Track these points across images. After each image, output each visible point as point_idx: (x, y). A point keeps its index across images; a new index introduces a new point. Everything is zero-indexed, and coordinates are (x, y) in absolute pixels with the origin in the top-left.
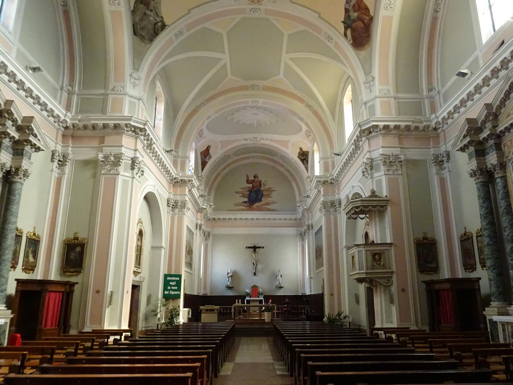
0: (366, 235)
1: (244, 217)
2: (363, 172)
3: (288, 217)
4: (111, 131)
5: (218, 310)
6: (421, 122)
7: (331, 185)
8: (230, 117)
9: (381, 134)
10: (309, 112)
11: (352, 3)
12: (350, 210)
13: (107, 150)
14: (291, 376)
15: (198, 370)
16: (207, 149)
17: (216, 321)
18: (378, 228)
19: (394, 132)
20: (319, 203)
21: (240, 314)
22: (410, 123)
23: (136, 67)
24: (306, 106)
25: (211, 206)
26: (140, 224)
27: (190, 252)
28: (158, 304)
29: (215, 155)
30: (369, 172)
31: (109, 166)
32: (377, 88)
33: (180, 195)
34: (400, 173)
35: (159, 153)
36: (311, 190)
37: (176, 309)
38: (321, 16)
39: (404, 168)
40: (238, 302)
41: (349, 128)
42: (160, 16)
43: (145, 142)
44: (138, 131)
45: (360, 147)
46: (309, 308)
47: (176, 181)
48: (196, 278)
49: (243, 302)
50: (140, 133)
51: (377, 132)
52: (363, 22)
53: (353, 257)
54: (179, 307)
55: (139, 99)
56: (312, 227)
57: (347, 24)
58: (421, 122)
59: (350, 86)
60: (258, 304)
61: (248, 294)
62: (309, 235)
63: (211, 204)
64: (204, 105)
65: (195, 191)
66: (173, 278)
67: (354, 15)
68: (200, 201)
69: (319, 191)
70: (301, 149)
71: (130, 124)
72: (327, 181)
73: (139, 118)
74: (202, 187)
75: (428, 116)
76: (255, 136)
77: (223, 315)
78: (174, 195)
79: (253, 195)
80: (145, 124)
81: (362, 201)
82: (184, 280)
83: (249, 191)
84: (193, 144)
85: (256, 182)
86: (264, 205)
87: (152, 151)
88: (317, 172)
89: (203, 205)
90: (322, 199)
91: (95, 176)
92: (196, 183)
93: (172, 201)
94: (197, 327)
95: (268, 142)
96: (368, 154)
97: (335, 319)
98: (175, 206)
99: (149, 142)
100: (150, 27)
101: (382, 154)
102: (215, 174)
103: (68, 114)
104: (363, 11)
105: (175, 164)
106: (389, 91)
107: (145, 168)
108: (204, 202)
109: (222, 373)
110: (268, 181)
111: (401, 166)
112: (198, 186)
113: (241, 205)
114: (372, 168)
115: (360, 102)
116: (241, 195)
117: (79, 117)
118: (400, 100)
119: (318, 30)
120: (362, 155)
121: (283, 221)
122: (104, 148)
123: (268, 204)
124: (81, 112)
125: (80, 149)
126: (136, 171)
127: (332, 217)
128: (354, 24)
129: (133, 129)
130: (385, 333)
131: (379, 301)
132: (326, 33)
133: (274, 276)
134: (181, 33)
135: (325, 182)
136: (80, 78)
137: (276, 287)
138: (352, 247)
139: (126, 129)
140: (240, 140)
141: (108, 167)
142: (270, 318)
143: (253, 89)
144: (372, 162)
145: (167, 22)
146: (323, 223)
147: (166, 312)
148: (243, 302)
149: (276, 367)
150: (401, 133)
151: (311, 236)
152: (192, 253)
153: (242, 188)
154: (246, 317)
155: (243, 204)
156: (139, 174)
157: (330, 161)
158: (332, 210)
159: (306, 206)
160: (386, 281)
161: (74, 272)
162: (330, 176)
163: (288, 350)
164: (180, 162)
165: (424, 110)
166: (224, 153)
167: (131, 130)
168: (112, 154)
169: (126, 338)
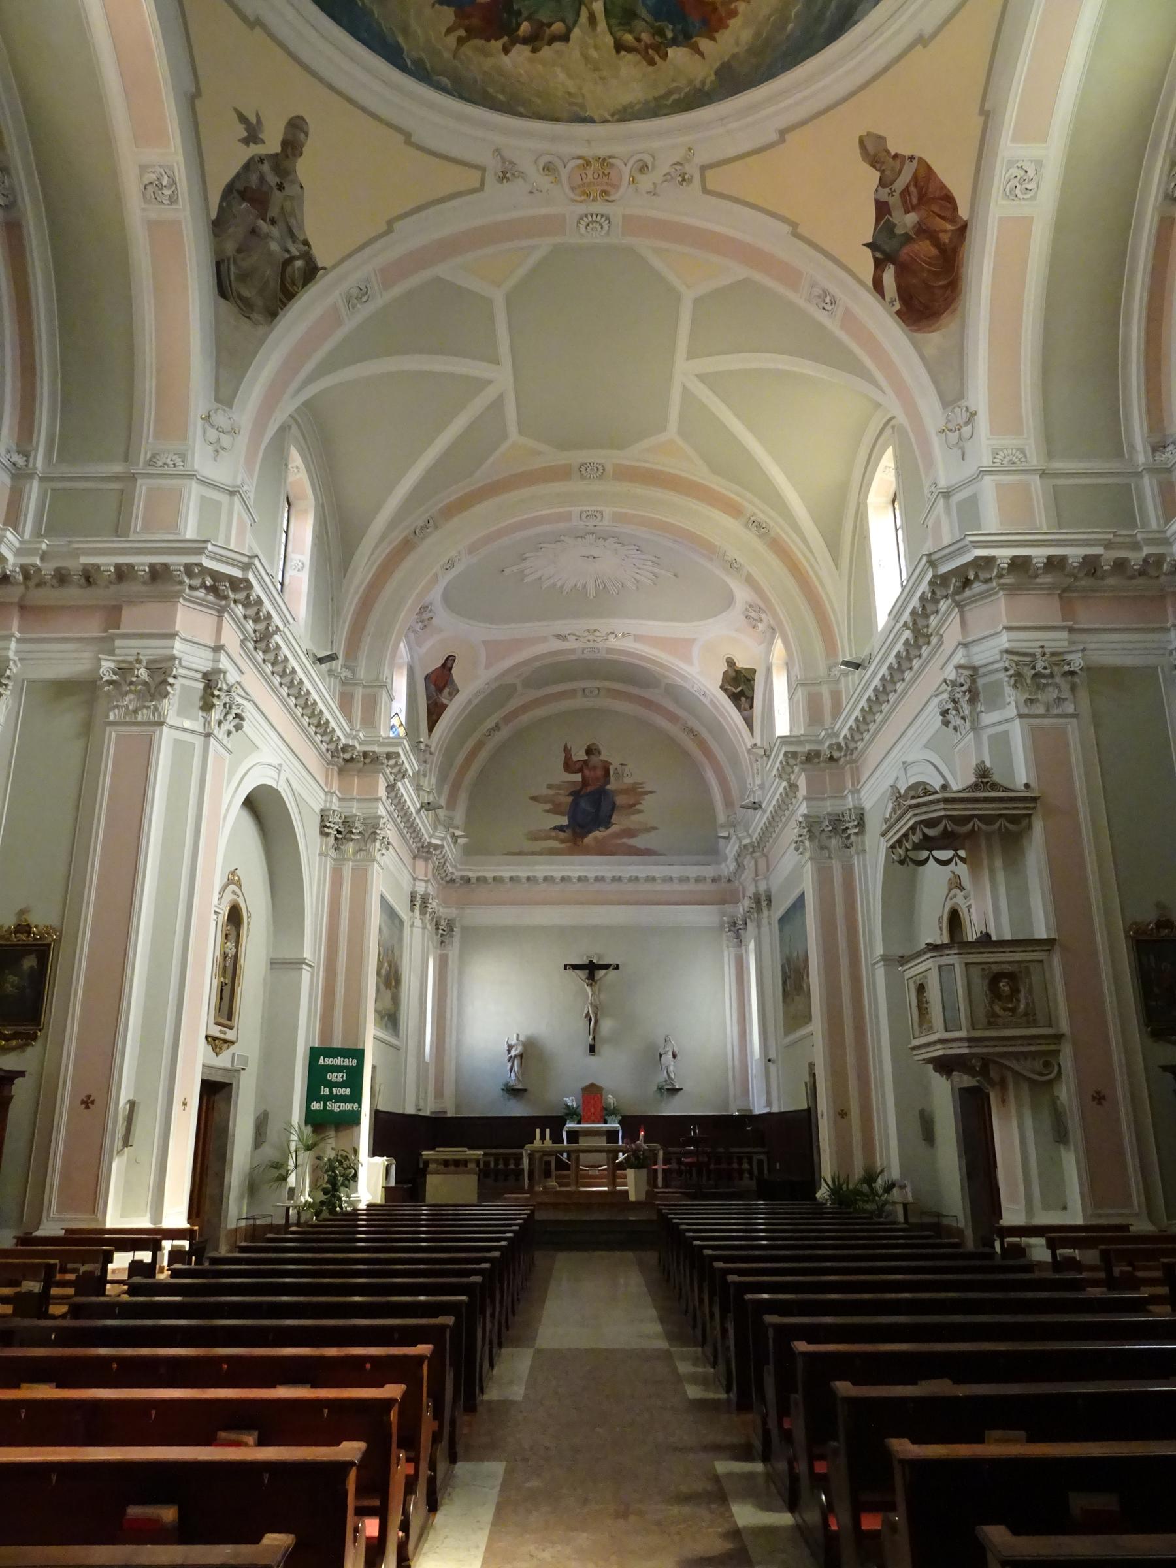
0: (955, 920)
1: (558, 875)
2: (945, 713)
3: (693, 871)
4: (144, 589)
5: (478, 1162)
6: (1136, 546)
7: (834, 764)
8: (515, 569)
9: (1003, 587)
10: (760, 546)
11: (899, 185)
12: (906, 835)
13: (127, 648)
14: (743, 1405)
15: (393, 1415)
16: (444, 665)
17: (473, 1198)
18: (1002, 890)
19: (1046, 579)
20: (793, 824)
21: (547, 1175)
22: (1098, 550)
23: (225, 392)
24: (746, 526)
25: (455, 838)
26: (232, 887)
27: (391, 979)
28: (289, 1141)
29: (470, 684)
30: (966, 710)
31: (132, 696)
32: (985, 443)
33: (358, 800)
34: (1070, 709)
35: (293, 662)
36: (762, 787)
37: (346, 1158)
38: (800, 230)
39: (1083, 695)
40: (543, 1138)
41: (889, 579)
42: (302, 238)
43: (250, 626)
44: (225, 590)
45: (929, 636)
46: (764, 1157)
47: (347, 756)
48: (411, 1060)
49: (557, 1138)
50: (232, 596)
51: (988, 581)
52: (936, 241)
53: (921, 989)
54: (356, 1152)
55: (232, 493)
56: (769, 899)
57: (883, 252)
58: (1136, 546)
59: (890, 452)
60: (602, 1143)
61: (571, 1113)
62: (759, 927)
63: (458, 833)
64: (436, 527)
65: (406, 789)
66: (338, 1061)
67: (907, 221)
68: (423, 822)
69: (793, 787)
70: (731, 663)
71: (199, 565)
72: (818, 754)
73: (232, 547)
74: (430, 782)
75: (1154, 525)
76: (592, 628)
77: (496, 1179)
78: (340, 799)
79: (584, 804)
80: (246, 567)
81: (947, 801)
82: (374, 1067)
83: (571, 794)
84: (402, 647)
85: (594, 768)
86: (619, 835)
87: (271, 656)
88: (782, 726)
89: (430, 837)
90: (803, 809)
91: (87, 728)
92: (410, 763)
93: (336, 819)
94: (415, 1220)
95: (629, 645)
96: (961, 652)
97: (857, 1192)
98: (343, 833)
99: (261, 626)
100: (269, 273)
101: (1008, 652)
102: (470, 744)
103: (8, 534)
104: (936, 209)
105: (345, 704)
106: (1022, 451)
107: (249, 706)
108: (435, 829)
109: (492, 1394)
110: (630, 767)
111: (1073, 688)
112: (417, 774)
113: (549, 838)
114: (974, 696)
115: (926, 490)
116: (548, 806)
117: (44, 546)
118: (1061, 481)
119: (790, 275)
120: (939, 659)
121: (676, 887)
122: (118, 643)
123: (630, 833)
124: (51, 531)
125: (46, 646)
126: (216, 714)
127: (836, 865)
128: (905, 250)
129: (209, 582)
130: (1052, 1245)
131: (1012, 1136)
132: (813, 285)
133: (654, 1056)
134: (363, 294)
135: (811, 758)
136: (52, 426)
137: (660, 1089)
138: (919, 954)
139: (186, 580)
140: (544, 639)
141: (130, 701)
142: (644, 1188)
143: (583, 477)
144: (973, 678)
145: (322, 257)
146: (808, 884)
147: (314, 1169)
148: (557, 1138)
149: (684, 1368)
150: (1069, 582)
151: (765, 929)
152: (398, 982)
153: (550, 787)
154: (568, 1185)
155: (553, 834)
156: (228, 725)
157: (825, 691)
158: (834, 842)
159: (750, 836)
160: (1038, 1065)
161: (15, 1036)
162: (829, 736)
163: (724, 1311)
164: (362, 698)
165: (1140, 508)
166: (497, 678)
167: (203, 585)
168: (144, 659)
169: (175, 1255)
